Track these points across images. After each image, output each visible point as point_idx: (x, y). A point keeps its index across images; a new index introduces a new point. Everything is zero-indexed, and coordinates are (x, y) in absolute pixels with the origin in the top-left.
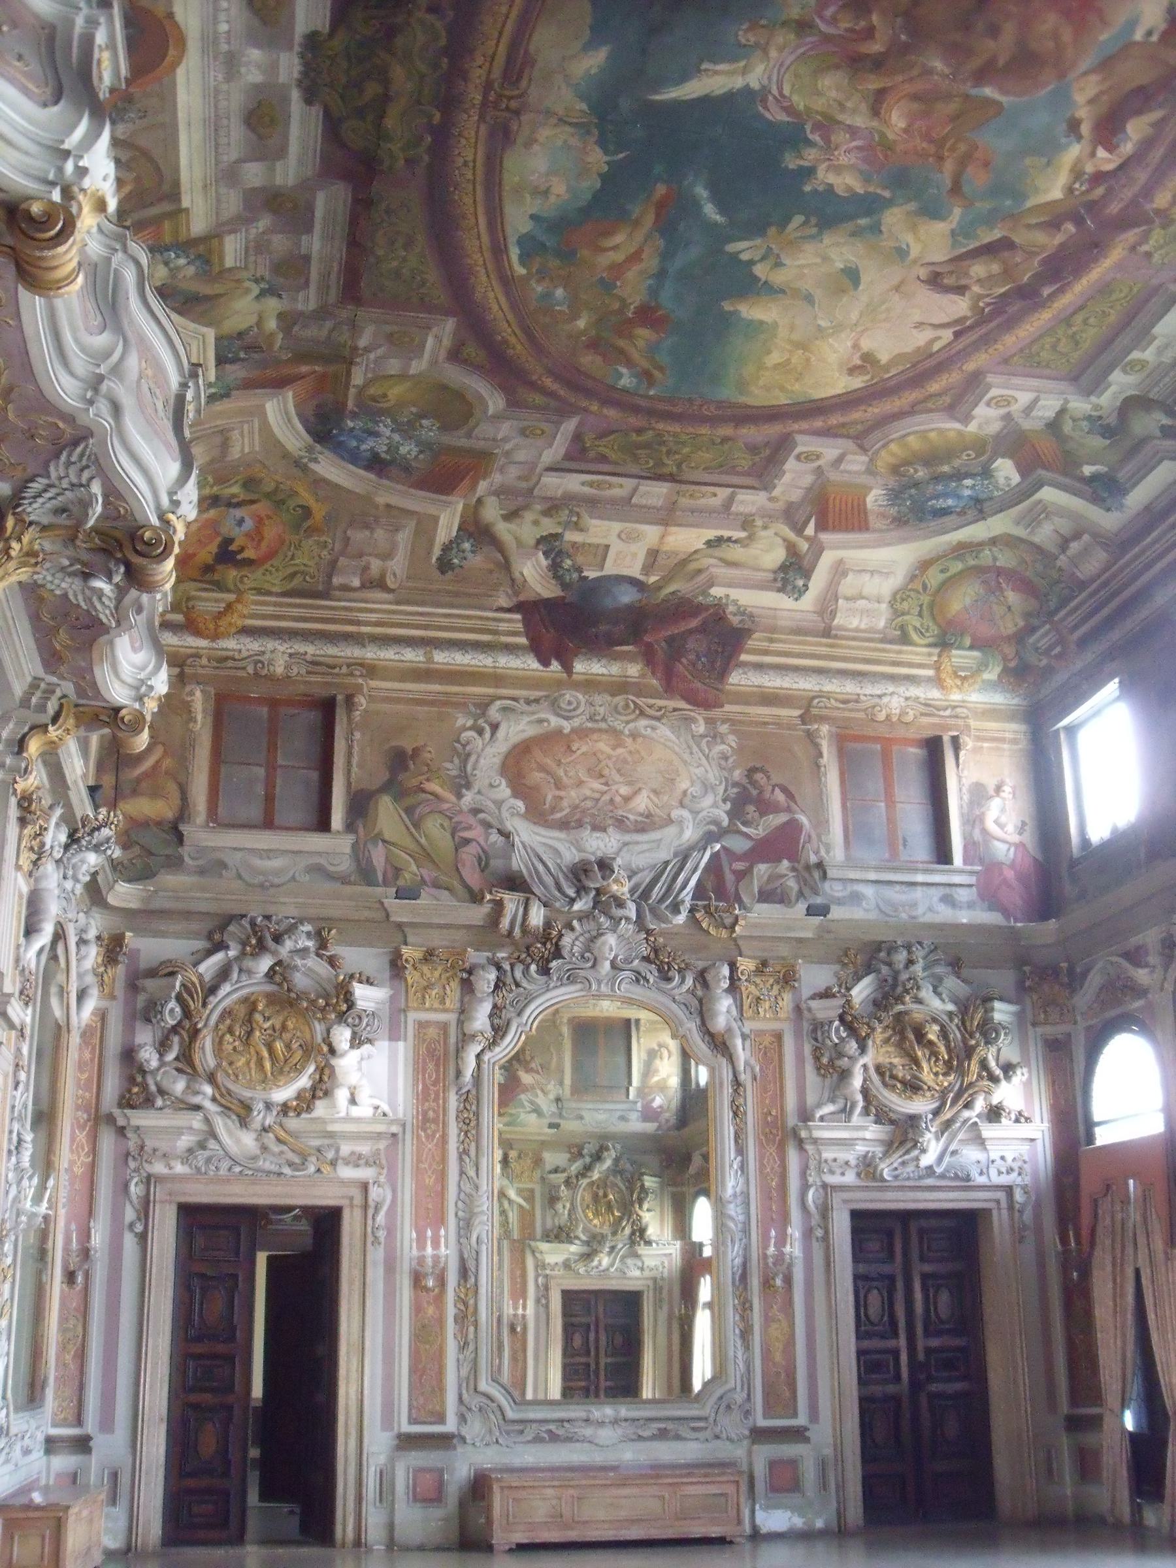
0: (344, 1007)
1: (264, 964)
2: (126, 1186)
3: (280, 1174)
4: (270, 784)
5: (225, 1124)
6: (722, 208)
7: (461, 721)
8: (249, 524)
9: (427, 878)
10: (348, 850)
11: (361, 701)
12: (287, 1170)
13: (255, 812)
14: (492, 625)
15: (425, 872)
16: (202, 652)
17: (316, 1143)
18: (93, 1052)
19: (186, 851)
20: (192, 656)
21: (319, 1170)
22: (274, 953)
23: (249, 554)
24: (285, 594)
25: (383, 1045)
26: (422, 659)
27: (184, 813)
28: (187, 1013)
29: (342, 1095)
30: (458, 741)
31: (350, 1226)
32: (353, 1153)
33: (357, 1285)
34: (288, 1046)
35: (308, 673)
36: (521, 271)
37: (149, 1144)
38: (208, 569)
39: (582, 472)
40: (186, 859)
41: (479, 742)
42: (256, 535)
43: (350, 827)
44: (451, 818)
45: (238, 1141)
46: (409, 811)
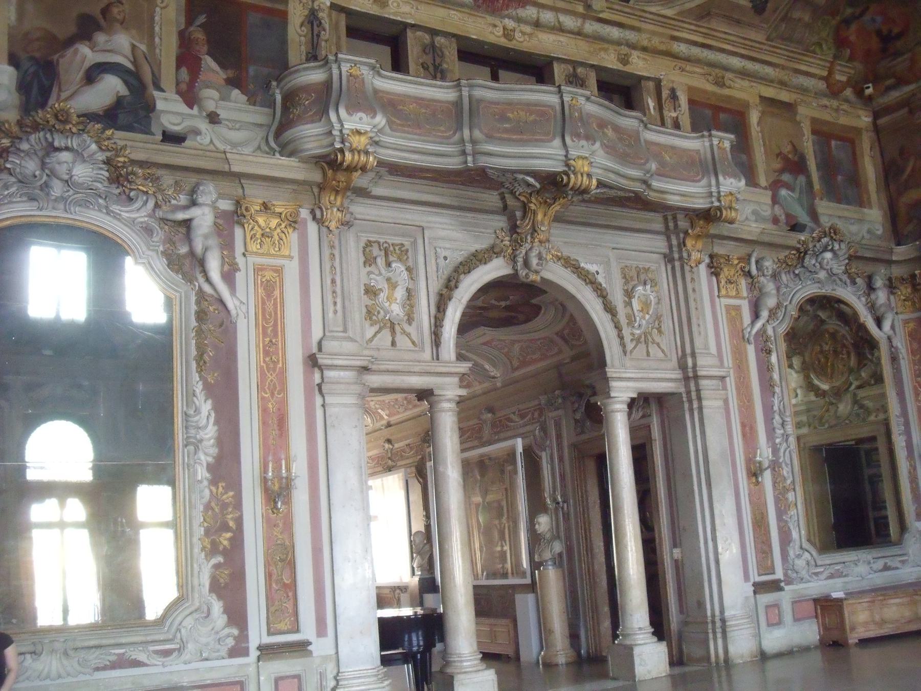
23: (896, 30)
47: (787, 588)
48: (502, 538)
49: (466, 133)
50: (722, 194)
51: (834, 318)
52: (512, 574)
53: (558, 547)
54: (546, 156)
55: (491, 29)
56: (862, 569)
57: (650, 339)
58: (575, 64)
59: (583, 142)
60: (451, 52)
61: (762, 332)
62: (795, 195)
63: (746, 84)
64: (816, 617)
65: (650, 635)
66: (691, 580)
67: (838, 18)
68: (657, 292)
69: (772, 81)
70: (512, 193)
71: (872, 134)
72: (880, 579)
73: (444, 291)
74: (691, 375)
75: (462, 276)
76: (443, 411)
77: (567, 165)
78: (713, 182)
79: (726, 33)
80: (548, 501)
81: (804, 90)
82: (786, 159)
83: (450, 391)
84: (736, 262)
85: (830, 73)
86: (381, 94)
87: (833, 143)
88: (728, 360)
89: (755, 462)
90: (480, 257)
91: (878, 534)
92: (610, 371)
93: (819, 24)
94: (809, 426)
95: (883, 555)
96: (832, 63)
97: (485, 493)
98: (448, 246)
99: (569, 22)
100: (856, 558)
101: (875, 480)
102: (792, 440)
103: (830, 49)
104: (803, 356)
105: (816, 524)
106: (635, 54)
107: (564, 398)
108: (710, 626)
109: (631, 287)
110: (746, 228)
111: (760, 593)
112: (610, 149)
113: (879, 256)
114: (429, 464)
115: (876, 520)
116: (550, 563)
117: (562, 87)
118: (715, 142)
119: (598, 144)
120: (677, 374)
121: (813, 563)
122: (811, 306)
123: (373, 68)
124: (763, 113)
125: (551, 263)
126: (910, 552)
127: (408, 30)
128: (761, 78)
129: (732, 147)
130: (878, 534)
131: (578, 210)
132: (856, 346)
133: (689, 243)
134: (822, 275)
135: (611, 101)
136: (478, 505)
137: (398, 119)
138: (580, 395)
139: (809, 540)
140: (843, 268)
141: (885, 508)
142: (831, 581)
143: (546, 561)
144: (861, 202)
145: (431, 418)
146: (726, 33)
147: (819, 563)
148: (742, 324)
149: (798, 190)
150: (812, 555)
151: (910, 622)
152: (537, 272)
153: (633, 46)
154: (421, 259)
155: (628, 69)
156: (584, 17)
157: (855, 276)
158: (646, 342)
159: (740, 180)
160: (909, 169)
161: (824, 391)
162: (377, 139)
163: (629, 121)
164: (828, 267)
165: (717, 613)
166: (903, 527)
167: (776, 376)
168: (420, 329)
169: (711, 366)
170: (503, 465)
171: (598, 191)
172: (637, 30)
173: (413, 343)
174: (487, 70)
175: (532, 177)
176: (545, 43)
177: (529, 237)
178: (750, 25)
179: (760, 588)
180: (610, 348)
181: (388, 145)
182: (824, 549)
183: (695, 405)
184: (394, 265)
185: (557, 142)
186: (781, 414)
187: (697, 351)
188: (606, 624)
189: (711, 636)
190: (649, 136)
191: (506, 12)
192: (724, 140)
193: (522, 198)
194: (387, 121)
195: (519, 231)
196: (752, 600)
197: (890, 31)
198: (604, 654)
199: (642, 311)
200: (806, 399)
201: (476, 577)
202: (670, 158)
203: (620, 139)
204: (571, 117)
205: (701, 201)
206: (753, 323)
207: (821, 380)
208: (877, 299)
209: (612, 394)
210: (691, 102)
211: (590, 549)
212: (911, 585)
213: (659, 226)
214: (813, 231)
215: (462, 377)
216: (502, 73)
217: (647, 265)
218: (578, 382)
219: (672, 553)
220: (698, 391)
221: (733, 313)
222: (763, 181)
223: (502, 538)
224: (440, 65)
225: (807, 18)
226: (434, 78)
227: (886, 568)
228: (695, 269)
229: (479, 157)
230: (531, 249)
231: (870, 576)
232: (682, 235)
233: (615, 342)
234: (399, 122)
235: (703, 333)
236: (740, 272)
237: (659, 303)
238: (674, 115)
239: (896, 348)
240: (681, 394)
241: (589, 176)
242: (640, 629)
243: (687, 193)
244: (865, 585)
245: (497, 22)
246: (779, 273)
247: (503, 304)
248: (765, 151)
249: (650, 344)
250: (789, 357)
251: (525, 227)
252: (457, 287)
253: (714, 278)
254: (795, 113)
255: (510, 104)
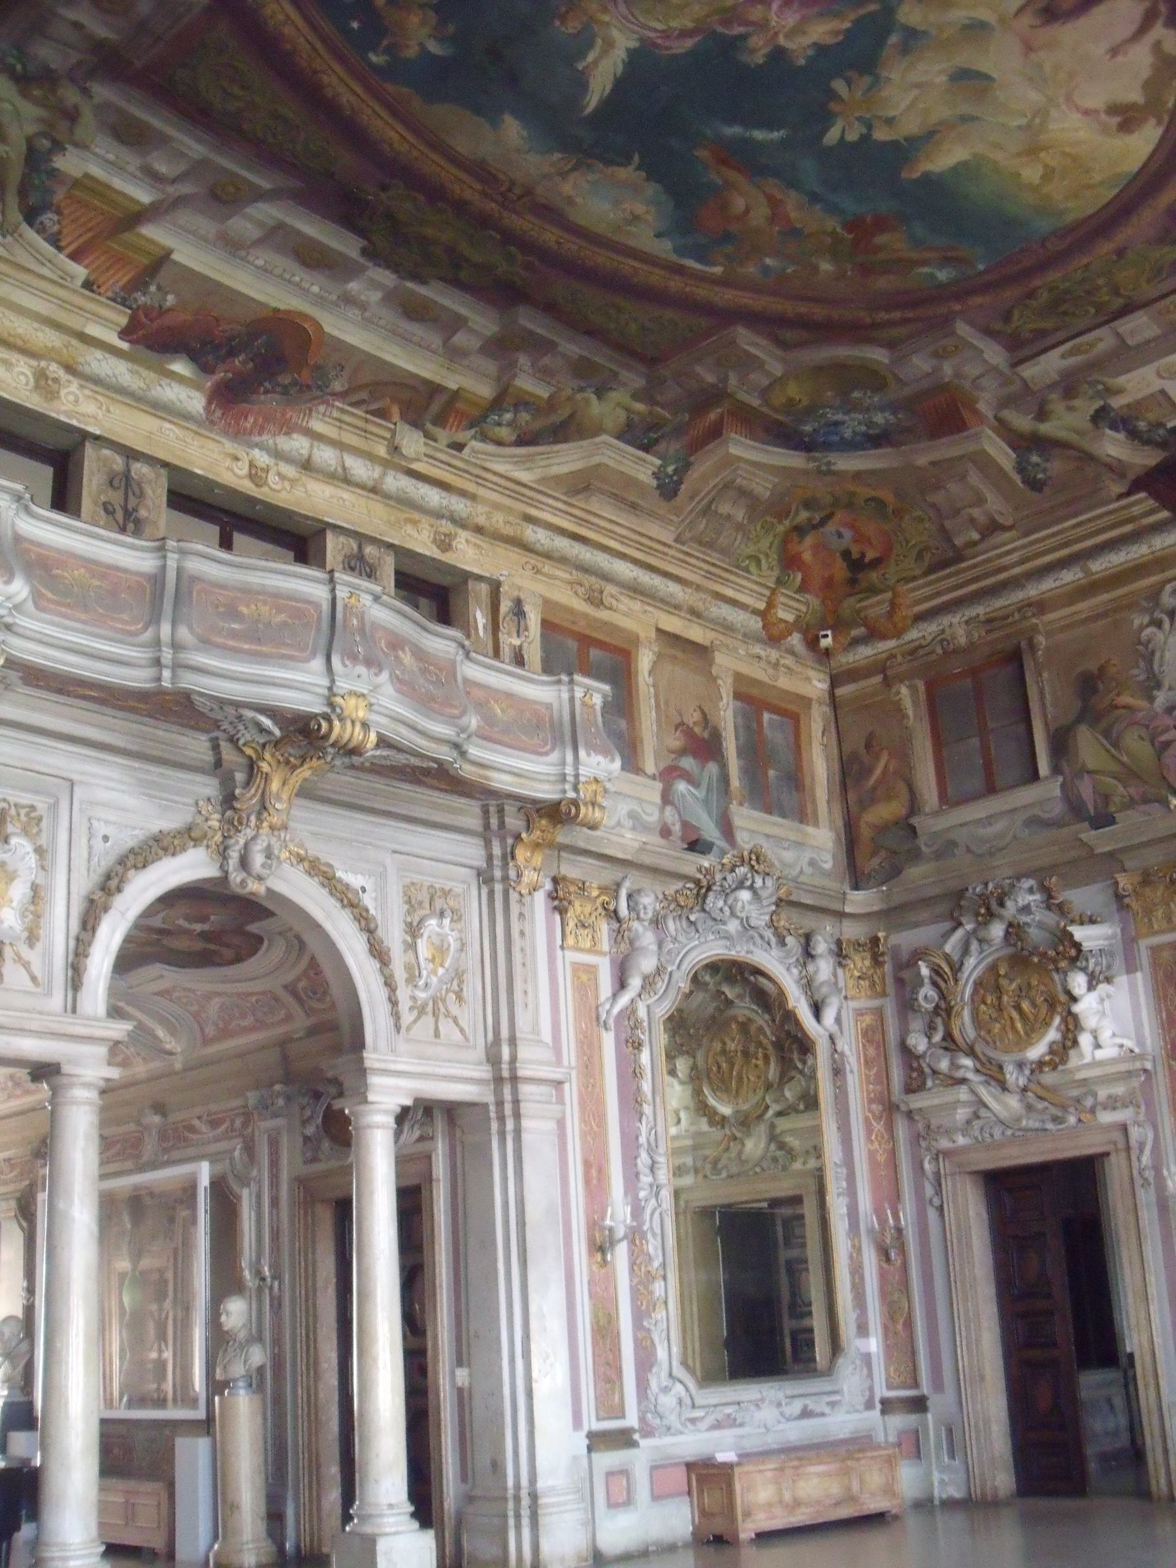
0: (1073, 952)
1: (997, 931)
2: (922, 1168)
3: (1046, 1130)
4: (985, 749)
5: (989, 1092)
6: (770, 126)
7: (1137, 622)
8: (848, 534)
9: (1136, 797)
10: (1058, 792)
11: (1041, 639)
12: (1050, 1126)
13: (976, 782)
14: (1125, 514)
15: (1132, 790)
16: (893, 652)
17: (1075, 1093)
18: (878, 1048)
19: (922, 841)
20: (889, 658)
21: (1080, 1120)
22: (1001, 917)
23: (870, 555)
24: (926, 573)
25: (1122, 980)
26: (1080, 575)
27: (914, 807)
28: (943, 996)
29: (1085, 1040)
30: (1140, 643)
31: (1115, 1173)
32: (1110, 1097)
33: (1133, 1232)
34: (1034, 1004)
35: (988, 632)
36: (718, 270)
37: (934, 1123)
38: (852, 582)
39: (1054, 346)
40: (924, 848)
41: (1160, 636)
42: (859, 538)
43: (1056, 770)
44: (1147, 727)
45: (1005, 1106)
46: (1107, 734)
47: (643, 1443)
48: (162, 1336)
49: (166, 629)
50: (582, 779)
51: (747, 999)
52: (175, 1400)
53: (258, 1356)
54: (297, 685)
55: (228, 462)
56: (768, 1414)
57: (442, 1010)
58: (362, 538)
59: (361, 669)
60: (156, 492)
61: (630, 1012)
62: (700, 794)
63: (637, 606)
64: (689, 1493)
65: (407, 1517)
66: (481, 1422)
67: (787, 523)
68: (460, 931)
69: (677, 607)
70: (233, 740)
71: (826, 709)
72: (795, 1432)
73: (98, 895)
74: (506, 1074)
75: (132, 872)
76: (74, 1103)
77: (331, 705)
78: (569, 757)
79: (611, 521)
80: (247, 1274)
81: (727, 628)
82: (689, 733)
83: (90, 1069)
84: (595, 893)
85: (770, 605)
86: (26, 545)
87: (766, 716)
88: (570, 1055)
89: (602, 1229)
90: (165, 843)
91: (796, 1358)
92: (371, 1058)
93: (758, 527)
94: (696, 1171)
95: (801, 1391)
96: (773, 591)
97: (136, 1256)
98: (112, 818)
99: (360, 469)
100: (759, 1396)
101: (796, 1268)
102: (666, 1195)
103: (771, 568)
104: (694, 1057)
105: (697, 1339)
106: (463, 535)
107: (288, 1099)
108: (511, 1505)
109: (417, 919)
110: (614, 838)
111: (599, 1450)
112: (405, 686)
113: (824, 903)
114: (42, 1197)
115: (794, 1335)
116: (241, 1384)
117: (337, 575)
118: (579, 693)
119: (385, 676)
120: (484, 1072)
121: (689, 1402)
122: (712, 976)
123: (19, 498)
124: (660, 656)
125: (286, 866)
126: (845, 1389)
127: (87, 444)
128: (662, 601)
129: (605, 705)
130: (796, 1358)
131: (342, 781)
132: (779, 1046)
133: (521, 854)
134: (733, 926)
135: (416, 606)
136: (122, 1276)
137: (51, 591)
138: (317, 1096)
139: (684, 1363)
140: (767, 918)
141: (810, 1313)
142: (716, 1434)
143: (235, 1380)
144: (803, 815)
145: (53, 1113)
146: (611, 521)
147: (699, 1401)
148: (597, 997)
149: (704, 786)
150: (687, 1390)
151: (837, 1504)
152: (260, 878)
153: (462, 524)
154: (63, 837)
155: (448, 558)
156: (386, 464)
157: (785, 933)
158: (435, 1014)
159: (613, 760)
160: (878, 771)
161: (724, 1118)
162: (9, 620)
163: (440, 643)
164: (744, 915)
165: (524, 1482)
166: (836, 1347)
167: (646, 1087)
168: (48, 955)
169: (542, 1063)
170: (174, 1208)
171: (378, 753)
172: (473, 497)
173: (34, 979)
174: (214, 530)
175: (269, 717)
176: (313, 498)
177: (253, 818)
178: (651, 514)
179: (598, 1441)
180: (374, 1021)
181: (28, 633)
182: (709, 1378)
183: (510, 1125)
184: (14, 841)
185: (318, 664)
186: (651, 1151)
187: (518, 1035)
188: (333, 1496)
189: (511, 1522)
190: (472, 671)
191: (257, 439)
192: (594, 693)
193: (249, 751)
194: (32, 592)
195: (237, 805)
196: (585, 1462)
197: (863, 555)
198: (325, 1550)
199: (433, 960)
200: (693, 1129)
201: (109, 1403)
202: (503, 711)
203: (424, 671)
204: (345, 626)
205: (546, 787)
206: (615, 996)
207: (719, 1099)
208: (816, 972)
209: (371, 1097)
210: (546, 624)
211: (313, 1365)
212: (844, 1442)
213: (475, 823)
214: (723, 853)
215: (115, 1046)
216: (238, 538)
217: (448, 885)
218: (314, 1069)
219: (453, 1374)
220: (516, 1102)
221: (584, 977)
222: (650, 766)
223: (162, 1336)
224: (135, 510)
225: (740, 514)
226: (123, 530)
227: (806, 1414)
228: (527, 899)
229: (181, 672)
230: (254, 838)
231: (781, 1427)
232: (510, 841)
233: (384, 1008)
234: (50, 595)
235: (530, 1006)
236: (600, 910)
237: (462, 950)
238: (516, 642)
239: (842, 1055)
240: (486, 1105)
241: (365, 726)
242: (391, 1506)
243: (526, 772)
244: (772, 1441)
245: (241, 453)
246: (665, 917)
247: (198, 927)
248: (658, 719)
249: (441, 1017)
250: (670, 1057)
251: (248, 799)
252: (119, 890)
253: (557, 917)
254: (711, 662)
255: (248, 592)
